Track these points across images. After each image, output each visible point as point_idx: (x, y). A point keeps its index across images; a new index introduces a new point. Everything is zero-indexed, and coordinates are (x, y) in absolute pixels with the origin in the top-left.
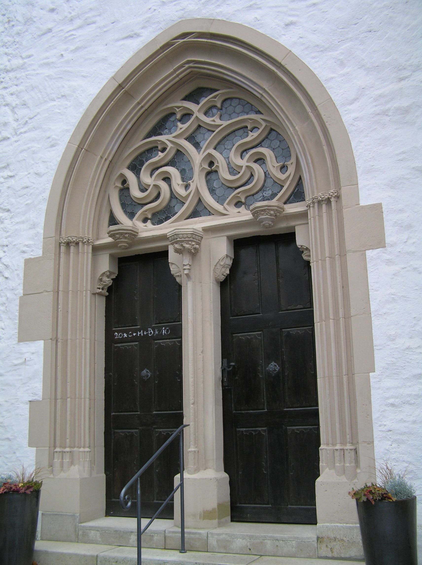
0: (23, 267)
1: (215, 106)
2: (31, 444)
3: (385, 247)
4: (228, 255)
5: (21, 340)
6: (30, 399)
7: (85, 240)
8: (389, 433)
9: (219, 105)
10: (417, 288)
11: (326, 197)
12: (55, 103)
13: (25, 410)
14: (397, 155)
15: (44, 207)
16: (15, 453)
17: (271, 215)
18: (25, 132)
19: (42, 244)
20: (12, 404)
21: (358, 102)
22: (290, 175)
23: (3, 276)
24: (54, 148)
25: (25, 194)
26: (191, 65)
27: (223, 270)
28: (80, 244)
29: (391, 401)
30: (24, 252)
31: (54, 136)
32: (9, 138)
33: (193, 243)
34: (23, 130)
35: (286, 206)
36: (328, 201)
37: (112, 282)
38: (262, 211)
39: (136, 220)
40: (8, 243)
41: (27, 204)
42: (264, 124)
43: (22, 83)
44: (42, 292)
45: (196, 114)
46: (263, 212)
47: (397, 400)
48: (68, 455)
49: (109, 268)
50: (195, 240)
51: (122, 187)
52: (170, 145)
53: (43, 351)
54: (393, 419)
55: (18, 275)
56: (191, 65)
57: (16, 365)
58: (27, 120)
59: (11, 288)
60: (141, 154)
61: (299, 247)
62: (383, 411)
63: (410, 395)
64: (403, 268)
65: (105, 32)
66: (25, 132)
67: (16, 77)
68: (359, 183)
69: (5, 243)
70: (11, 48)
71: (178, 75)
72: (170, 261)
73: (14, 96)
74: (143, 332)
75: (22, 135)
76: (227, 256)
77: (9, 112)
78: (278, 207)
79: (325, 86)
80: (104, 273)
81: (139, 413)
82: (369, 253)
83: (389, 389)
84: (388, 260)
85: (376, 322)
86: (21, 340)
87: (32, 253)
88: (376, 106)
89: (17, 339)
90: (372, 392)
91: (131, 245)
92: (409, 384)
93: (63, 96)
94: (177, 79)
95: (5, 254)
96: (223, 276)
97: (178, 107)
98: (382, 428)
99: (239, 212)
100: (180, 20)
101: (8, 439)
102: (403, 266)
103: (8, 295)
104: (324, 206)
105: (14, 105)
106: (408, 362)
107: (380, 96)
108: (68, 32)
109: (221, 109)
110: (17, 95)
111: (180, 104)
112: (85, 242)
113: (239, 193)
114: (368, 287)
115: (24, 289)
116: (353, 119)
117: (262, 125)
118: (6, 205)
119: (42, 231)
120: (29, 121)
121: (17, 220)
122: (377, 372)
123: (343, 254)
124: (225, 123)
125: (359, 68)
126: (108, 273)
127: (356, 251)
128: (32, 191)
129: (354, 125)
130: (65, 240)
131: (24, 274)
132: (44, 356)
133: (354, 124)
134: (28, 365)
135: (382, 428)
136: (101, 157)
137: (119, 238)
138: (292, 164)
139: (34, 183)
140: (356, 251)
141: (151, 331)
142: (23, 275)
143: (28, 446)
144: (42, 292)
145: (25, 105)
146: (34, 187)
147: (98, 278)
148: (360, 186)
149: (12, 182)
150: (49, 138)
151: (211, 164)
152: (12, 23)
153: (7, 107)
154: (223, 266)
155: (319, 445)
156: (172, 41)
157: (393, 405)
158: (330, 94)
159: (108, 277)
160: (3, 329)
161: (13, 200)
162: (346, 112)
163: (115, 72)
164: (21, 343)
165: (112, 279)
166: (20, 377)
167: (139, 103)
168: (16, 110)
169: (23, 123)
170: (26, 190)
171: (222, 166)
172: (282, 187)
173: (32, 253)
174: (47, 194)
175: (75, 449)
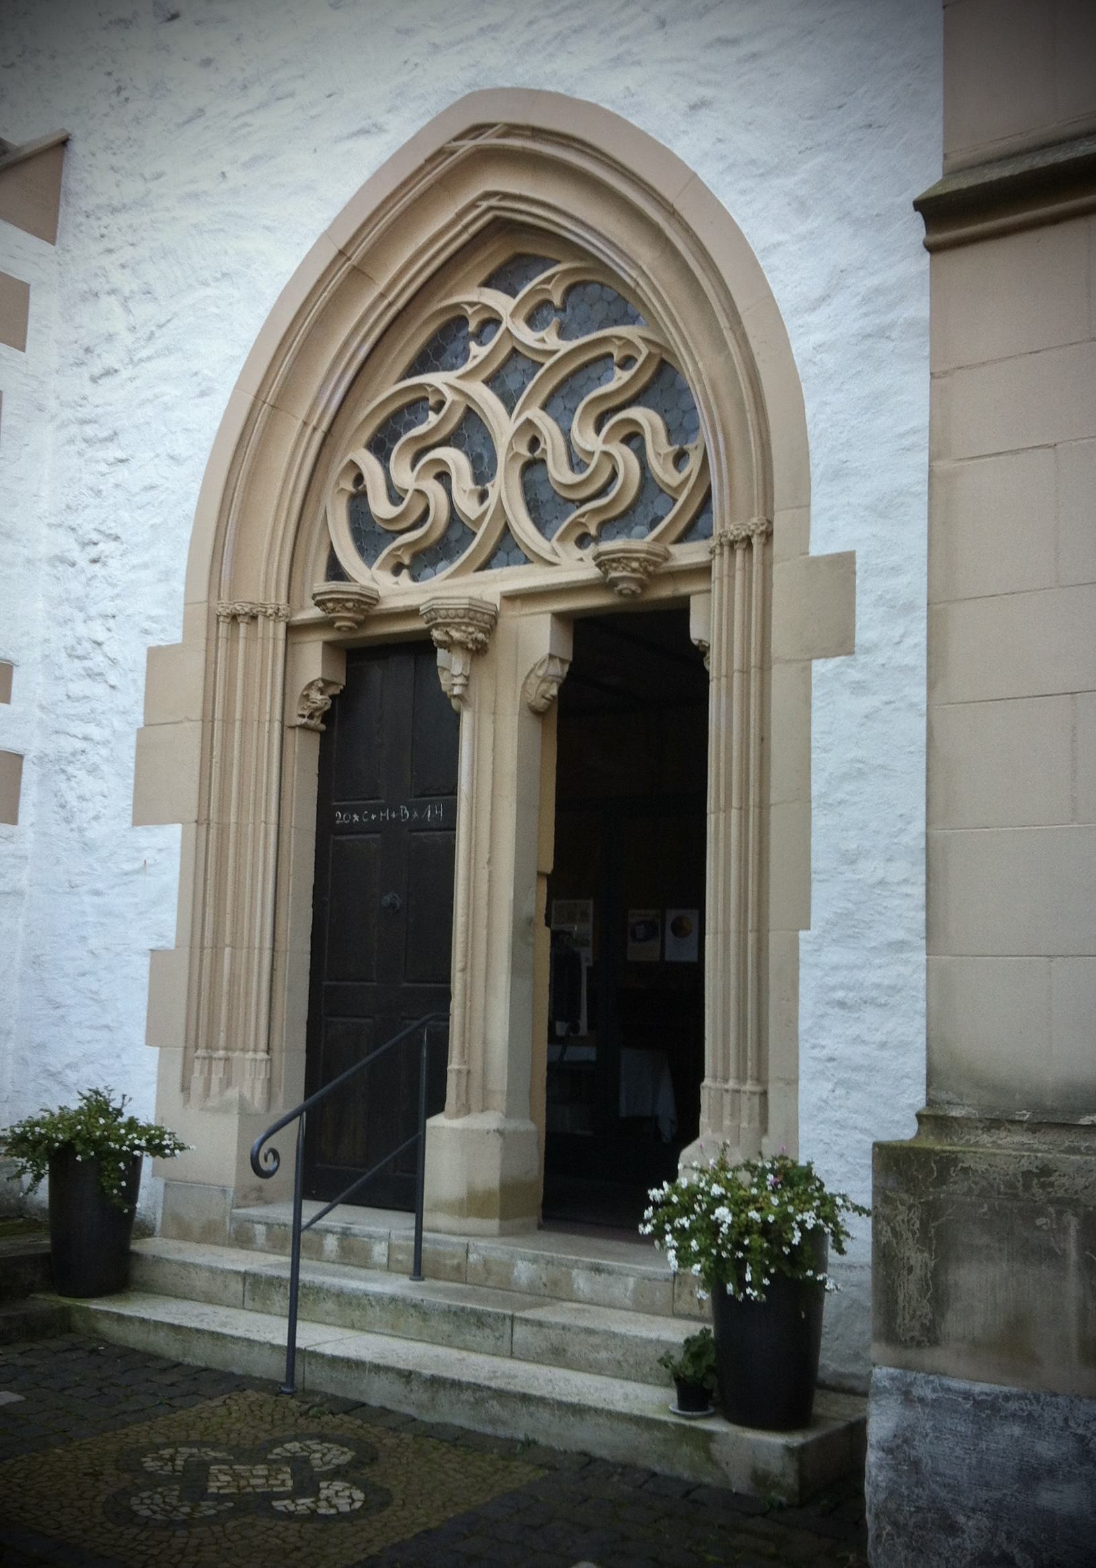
0: (145, 665)
1: (547, 303)
2: (150, 1041)
3: (851, 653)
4: (553, 653)
5: (138, 821)
6: (153, 945)
7: (270, 611)
8: (829, 1065)
9: (557, 300)
10: (912, 749)
11: (744, 534)
12: (209, 291)
13: (141, 967)
14: (902, 436)
15: (186, 534)
16: (118, 1056)
17: (634, 570)
18: (149, 358)
19: (181, 617)
20: (118, 954)
21: (829, 305)
22: (690, 475)
23: (106, 682)
24: (206, 399)
25: (149, 503)
26: (494, 202)
27: (544, 686)
28: (260, 618)
29: (840, 994)
30: (146, 632)
31: (206, 372)
32: (116, 371)
33: (471, 629)
34: (144, 354)
35: (675, 550)
36: (748, 540)
37: (330, 702)
38: (613, 560)
39: (379, 568)
40: (114, 612)
41: (152, 526)
42: (645, 350)
43: (143, 239)
44: (181, 722)
45: (507, 323)
46: (614, 565)
47: (851, 995)
48: (222, 1063)
49: (323, 672)
50: (475, 622)
51: (528, 454)
52: (450, 396)
53: (179, 845)
54: (841, 1036)
55: (134, 681)
56: (494, 202)
57: (126, 874)
58: (154, 328)
59: (121, 709)
60: (397, 415)
61: (696, 643)
62: (822, 1016)
63: (878, 986)
64: (887, 703)
65: (312, 118)
66: (149, 358)
67: (130, 226)
68: (812, 503)
69: (109, 611)
70: (122, 153)
71: (466, 228)
72: (439, 663)
73: (127, 271)
74: (391, 813)
75: (143, 364)
76: (551, 657)
77: (118, 310)
78: (648, 552)
79: (762, 264)
80: (311, 685)
81: (375, 984)
82: (820, 667)
83: (836, 968)
84: (858, 683)
85: (820, 821)
86: (138, 821)
87: (162, 636)
88: (866, 315)
89: (130, 819)
90: (803, 972)
91: (361, 624)
92: (877, 961)
93: (224, 275)
94: (465, 237)
95: (110, 634)
96: (544, 701)
97: (471, 304)
98: (816, 1053)
99: (581, 560)
100: (468, 91)
101: (107, 1027)
102: (885, 698)
103: (116, 724)
104: (739, 554)
105: (127, 294)
106: (880, 913)
107: (878, 291)
108: (237, 117)
109: (564, 309)
110: (133, 269)
111: (473, 297)
112: (271, 615)
113: (583, 515)
114: (810, 742)
115: (147, 713)
116: (814, 348)
117: (640, 352)
118: (113, 524)
119: (182, 589)
120: (158, 333)
121: (135, 560)
122: (815, 931)
123: (765, 667)
124: (566, 346)
125: (839, 219)
126: (321, 684)
127: (789, 661)
128: (162, 497)
129: (815, 363)
130: (228, 611)
131: (147, 679)
132: (182, 857)
133: (816, 360)
134: (150, 875)
135: (816, 1053)
136: (305, 424)
137: (333, 610)
138: (696, 448)
139: (167, 479)
140: (789, 661)
141: (406, 811)
142: (144, 682)
143: (143, 1042)
144: (181, 722)
145: (149, 293)
146: (167, 488)
147: (299, 694)
148: (814, 509)
149: (122, 473)
150: (196, 374)
151: (534, 443)
152: (124, 94)
153: (113, 297)
154: (544, 680)
155: (702, 1078)
156: (450, 145)
157: (842, 1004)
158: (771, 285)
159: (322, 691)
160: (104, 796)
161: (125, 515)
162: (801, 330)
163: (332, 220)
164: (139, 828)
165: (332, 697)
166: (136, 900)
167: (382, 296)
168: (130, 304)
169: (145, 337)
170: (152, 493)
171: (553, 449)
172: (675, 501)
173: (162, 636)
174: (191, 506)
175: (237, 1054)
